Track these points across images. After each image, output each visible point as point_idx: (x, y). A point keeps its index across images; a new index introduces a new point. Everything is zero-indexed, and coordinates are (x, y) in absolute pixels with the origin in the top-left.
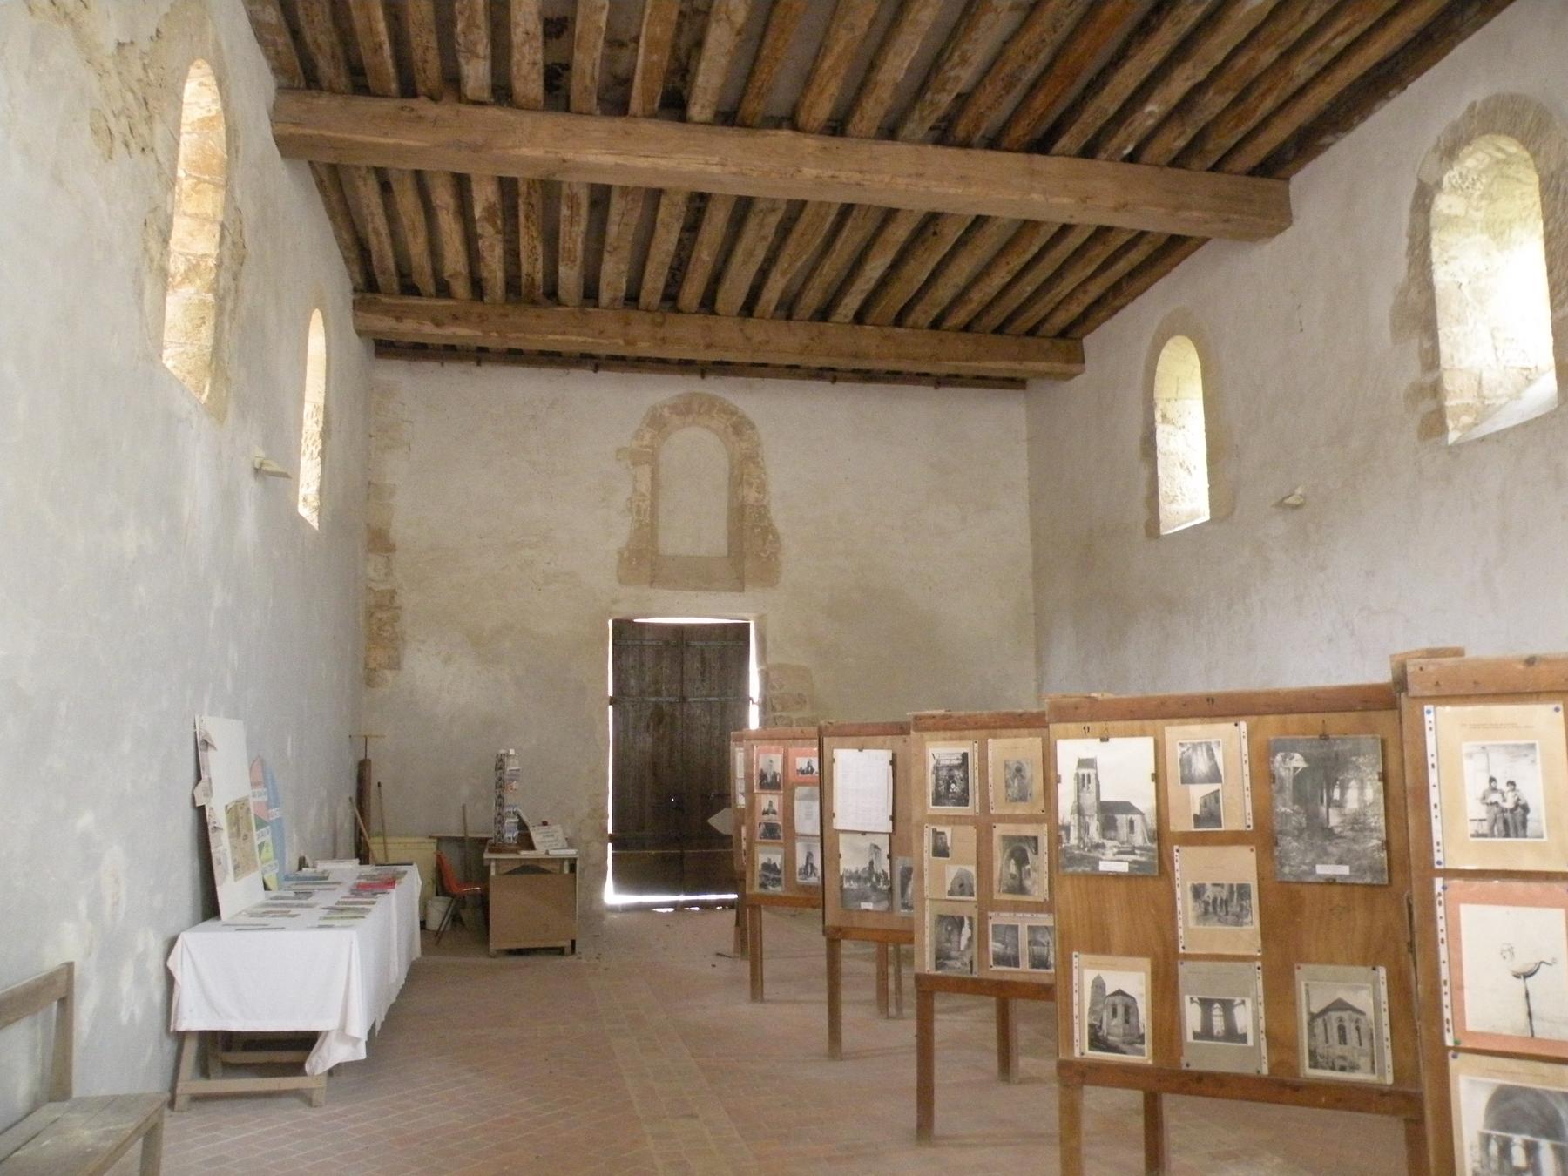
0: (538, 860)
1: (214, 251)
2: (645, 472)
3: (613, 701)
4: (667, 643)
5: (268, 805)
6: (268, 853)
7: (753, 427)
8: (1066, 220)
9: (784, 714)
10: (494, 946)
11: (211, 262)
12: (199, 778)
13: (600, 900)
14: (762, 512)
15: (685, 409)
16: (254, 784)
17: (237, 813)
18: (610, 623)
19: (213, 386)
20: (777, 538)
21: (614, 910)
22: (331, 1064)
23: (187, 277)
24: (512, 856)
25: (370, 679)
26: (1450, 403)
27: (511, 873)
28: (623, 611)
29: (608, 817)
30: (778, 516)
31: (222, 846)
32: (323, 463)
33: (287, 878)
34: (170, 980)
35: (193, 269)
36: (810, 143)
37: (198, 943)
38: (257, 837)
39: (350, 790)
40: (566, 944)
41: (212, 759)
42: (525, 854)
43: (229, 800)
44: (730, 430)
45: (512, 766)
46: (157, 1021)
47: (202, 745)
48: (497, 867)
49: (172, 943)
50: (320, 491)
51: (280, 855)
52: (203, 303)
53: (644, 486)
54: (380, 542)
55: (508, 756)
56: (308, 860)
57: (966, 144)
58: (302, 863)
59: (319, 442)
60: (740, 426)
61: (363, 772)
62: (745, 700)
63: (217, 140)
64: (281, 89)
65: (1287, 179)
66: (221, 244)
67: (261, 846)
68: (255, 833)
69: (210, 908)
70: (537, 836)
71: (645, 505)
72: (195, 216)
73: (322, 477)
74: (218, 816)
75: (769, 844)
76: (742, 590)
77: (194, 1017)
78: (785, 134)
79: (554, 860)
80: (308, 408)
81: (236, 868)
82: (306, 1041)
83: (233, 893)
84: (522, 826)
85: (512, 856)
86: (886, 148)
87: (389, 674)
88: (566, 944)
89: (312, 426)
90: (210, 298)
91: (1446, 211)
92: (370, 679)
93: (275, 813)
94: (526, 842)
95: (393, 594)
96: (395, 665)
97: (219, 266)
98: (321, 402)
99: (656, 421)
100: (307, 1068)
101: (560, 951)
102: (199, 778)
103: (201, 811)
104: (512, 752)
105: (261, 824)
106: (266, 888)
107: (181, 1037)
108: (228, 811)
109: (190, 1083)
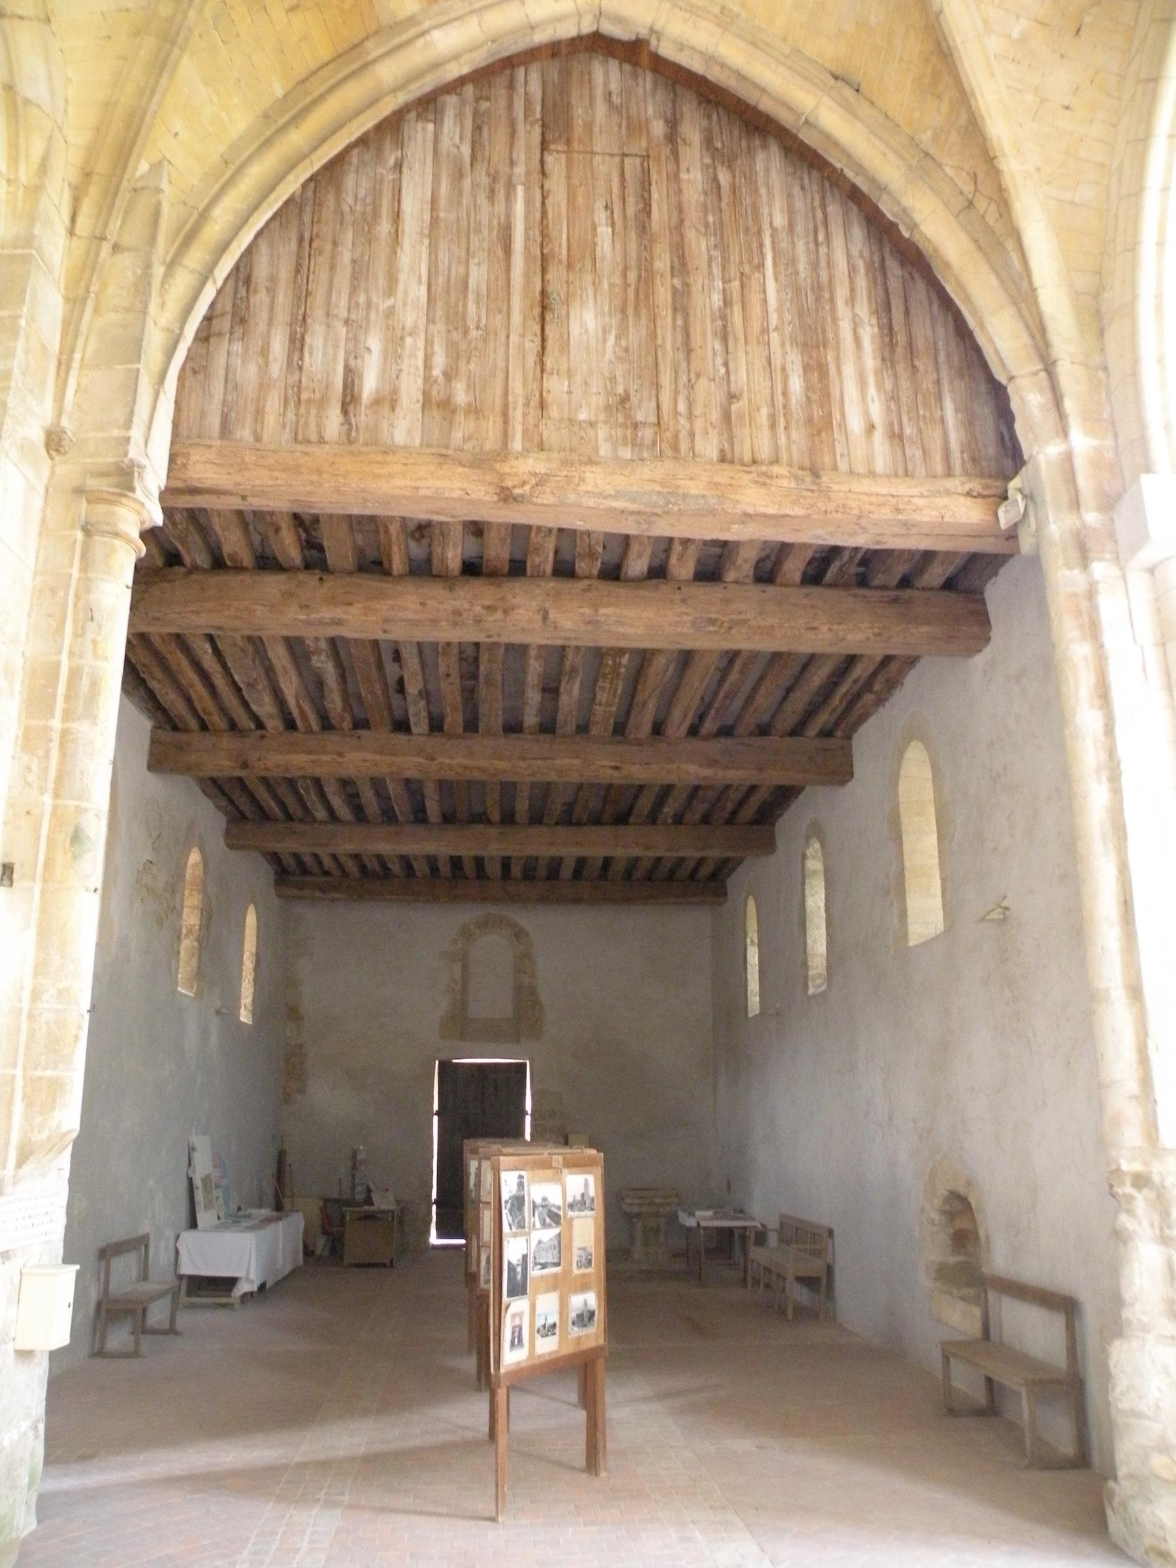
0: (374, 1212)
1: (198, 922)
2: (457, 967)
3: (437, 1113)
4: (473, 1076)
5: (222, 1177)
6: (221, 1201)
7: (527, 935)
8: (753, 782)
9: (542, 1123)
10: (345, 1262)
11: (197, 927)
12: (190, 1164)
13: (428, 1239)
14: (533, 992)
15: (486, 924)
16: (215, 1167)
17: (206, 1180)
18: (437, 1062)
19: (198, 984)
20: (542, 1008)
21: (435, 1247)
22: (242, 1292)
23: (187, 936)
24: (360, 1209)
25: (286, 1098)
26: (811, 973)
27: (359, 1219)
28: (444, 1055)
29: (432, 1187)
30: (544, 996)
31: (199, 1196)
32: (255, 984)
33: (230, 1216)
34: (177, 1252)
35: (190, 931)
36: (493, 831)
37: (188, 1237)
38: (216, 1193)
39: (272, 1168)
40: (387, 1261)
41: (196, 1156)
42: (366, 1208)
43: (203, 1175)
44: (513, 937)
45: (361, 1157)
46: (172, 1269)
47: (191, 1150)
48: (351, 1216)
49: (178, 1237)
50: (254, 1001)
51: (226, 1204)
52: (193, 947)
53: (458, 975)
54: (294, 1014)
55: (359, 1150)
56: (243, 1208)
57: (579, 824)
58: (239, 1209)
59: (253, 973)
60: (519, 934)
61: (281, 1159)
62: (524, 1113)
63: (200, 871)
64: (229, 822)
65: (773, 824)
66: (201, 920)
67: (217, 1198)
68: (214, 1191)
69: (193, 1224)
70: (375, 1198)
71: (459, 987)
72: (190, 907)
73: (254, 994)
74: (198, 1182)
75: (834, 1249)
76: (518, 1041)
77: (187, 1269)
78: (479, 828)
79: (383, 1212)
80: (247, 955)
81: (205, 1207)
82: (231, 1282)
83: (203, 1217)
84: (369, 1191)
85: (360, 1209)
86: (534, 831)
87: (298, 1097)
88: (387, 1261)
89: (248, 963)
90: (196, 944)
91: (812, 868)
92: (286, 1098)
93: (224, 1182)
94: (369, 1201)
95: (301, 1046)
96: (302, 1091)
97: (200, 929)
98: (254, 950)
99: (466, 934)
100: (233, 1295)
101: (384, 1265)
102: (190, 1164)
103: (190, 1180)
104: (361, 1148)
105: (217, 1187)
106: (219, 1218)
107: (181, 1277)
108: (202, 1180)
109: (184, 1299)
